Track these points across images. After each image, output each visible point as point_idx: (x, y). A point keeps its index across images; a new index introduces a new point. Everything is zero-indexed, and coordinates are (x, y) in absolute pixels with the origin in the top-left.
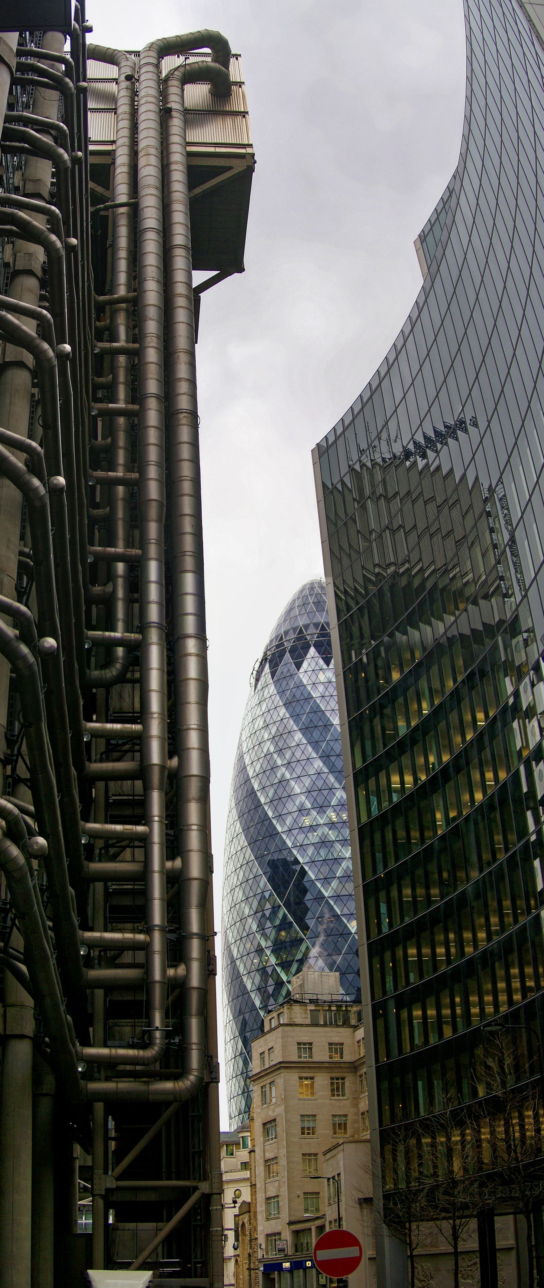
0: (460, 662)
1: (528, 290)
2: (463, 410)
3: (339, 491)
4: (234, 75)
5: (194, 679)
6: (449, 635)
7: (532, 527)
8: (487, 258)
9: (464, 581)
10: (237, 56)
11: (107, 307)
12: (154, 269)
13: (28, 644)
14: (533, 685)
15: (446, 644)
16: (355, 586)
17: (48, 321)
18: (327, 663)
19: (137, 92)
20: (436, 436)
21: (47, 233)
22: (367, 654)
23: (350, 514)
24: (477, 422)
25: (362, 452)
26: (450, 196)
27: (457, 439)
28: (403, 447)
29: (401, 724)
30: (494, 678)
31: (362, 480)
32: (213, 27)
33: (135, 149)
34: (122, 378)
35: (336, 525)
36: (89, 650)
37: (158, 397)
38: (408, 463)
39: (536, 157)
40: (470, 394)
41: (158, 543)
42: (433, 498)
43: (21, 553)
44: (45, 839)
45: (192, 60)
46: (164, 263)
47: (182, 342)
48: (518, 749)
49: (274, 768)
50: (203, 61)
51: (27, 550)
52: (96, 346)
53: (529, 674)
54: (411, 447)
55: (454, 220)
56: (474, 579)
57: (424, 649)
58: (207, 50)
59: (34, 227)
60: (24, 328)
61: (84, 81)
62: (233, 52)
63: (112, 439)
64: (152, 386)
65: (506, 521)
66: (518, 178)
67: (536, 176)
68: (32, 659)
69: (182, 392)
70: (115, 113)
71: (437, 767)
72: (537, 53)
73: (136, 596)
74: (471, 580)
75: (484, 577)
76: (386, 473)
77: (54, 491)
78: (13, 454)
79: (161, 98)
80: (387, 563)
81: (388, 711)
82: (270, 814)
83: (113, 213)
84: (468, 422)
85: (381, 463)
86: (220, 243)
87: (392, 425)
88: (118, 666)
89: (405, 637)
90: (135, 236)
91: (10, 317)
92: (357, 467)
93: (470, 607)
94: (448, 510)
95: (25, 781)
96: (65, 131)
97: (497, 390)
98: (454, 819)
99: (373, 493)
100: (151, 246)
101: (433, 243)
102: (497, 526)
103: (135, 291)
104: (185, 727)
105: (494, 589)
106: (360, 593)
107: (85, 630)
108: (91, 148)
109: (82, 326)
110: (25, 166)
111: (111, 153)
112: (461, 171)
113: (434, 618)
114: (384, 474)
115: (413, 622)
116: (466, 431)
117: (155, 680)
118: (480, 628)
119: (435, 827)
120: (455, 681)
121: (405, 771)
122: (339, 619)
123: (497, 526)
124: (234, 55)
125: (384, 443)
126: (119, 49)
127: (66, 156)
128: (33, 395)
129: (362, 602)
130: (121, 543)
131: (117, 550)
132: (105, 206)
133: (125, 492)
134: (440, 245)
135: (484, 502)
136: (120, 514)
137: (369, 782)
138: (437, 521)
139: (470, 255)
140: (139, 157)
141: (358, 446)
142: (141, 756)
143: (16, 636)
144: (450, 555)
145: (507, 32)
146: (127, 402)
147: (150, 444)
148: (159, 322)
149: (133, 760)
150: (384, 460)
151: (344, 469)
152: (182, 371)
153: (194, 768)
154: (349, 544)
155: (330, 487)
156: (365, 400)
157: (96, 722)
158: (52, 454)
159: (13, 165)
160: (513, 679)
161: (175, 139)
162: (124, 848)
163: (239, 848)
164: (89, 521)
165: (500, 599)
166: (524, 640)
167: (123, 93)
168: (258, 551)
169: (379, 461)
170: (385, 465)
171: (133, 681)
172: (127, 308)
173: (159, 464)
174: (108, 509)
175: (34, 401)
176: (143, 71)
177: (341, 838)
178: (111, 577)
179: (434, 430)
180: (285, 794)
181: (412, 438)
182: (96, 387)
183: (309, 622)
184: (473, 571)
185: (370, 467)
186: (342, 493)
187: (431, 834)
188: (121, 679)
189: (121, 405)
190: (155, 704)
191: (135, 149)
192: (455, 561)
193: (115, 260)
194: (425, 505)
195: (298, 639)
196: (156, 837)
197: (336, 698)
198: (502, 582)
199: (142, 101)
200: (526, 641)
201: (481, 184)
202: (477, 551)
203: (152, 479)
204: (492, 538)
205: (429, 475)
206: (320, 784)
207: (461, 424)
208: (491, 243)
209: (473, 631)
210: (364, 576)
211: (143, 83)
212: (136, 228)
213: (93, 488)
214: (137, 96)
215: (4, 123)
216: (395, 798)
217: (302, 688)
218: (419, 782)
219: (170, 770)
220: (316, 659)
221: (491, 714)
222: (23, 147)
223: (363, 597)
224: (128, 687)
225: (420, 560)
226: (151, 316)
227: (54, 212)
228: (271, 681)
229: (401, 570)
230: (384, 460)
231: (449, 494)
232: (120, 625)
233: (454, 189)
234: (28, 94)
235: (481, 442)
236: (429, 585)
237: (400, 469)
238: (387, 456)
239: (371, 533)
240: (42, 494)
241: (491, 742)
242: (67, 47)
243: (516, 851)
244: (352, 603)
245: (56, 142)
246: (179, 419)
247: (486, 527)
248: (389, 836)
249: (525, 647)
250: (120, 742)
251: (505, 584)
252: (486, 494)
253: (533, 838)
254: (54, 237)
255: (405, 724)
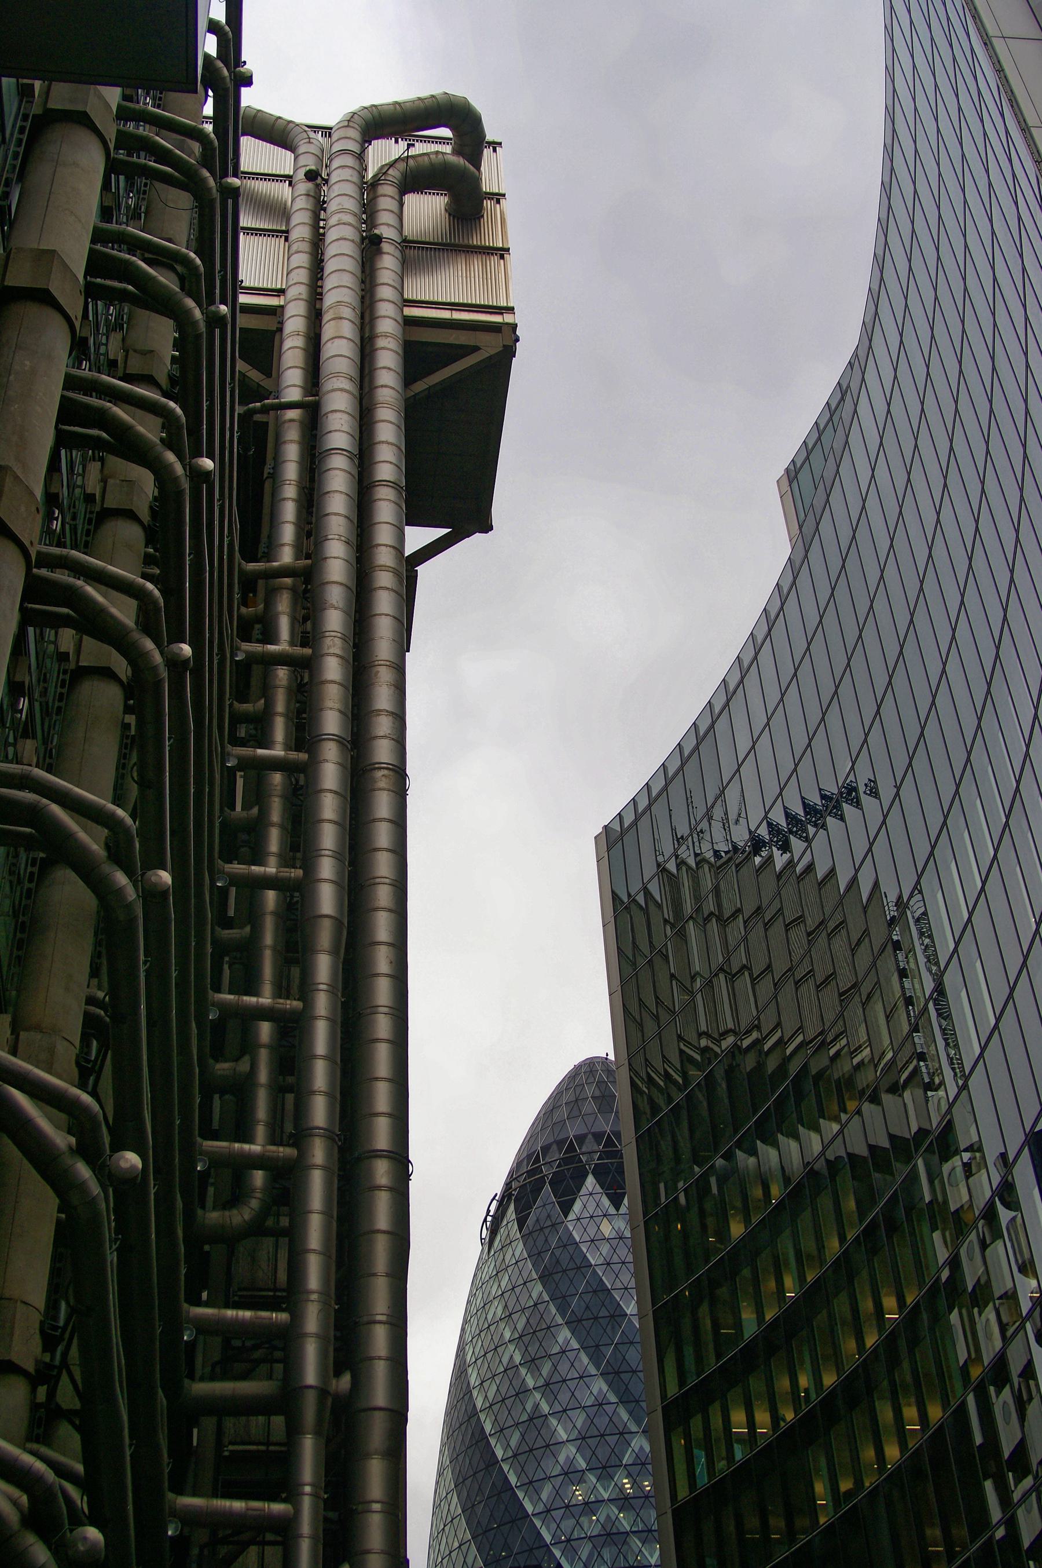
0: (850, 1204)
1: (970, 559)
2: (852, 768)
3: (641, 907)
4: (489, 183)
5: (384, 1232)
6: (830, 1155)
7: (975, 966)
8: (901, 507)
9: (855, 1061)
10: (495, 145)
11: (261, 583)
12: (341, 521)
13: (91, 1163)
14: (984, 1246)
15: (825, 1172)
16: (665, 1070)
17: (155, 602)
18: (617, 1203)
19: (324, 202)
20: (806, 813)
21: (160, 448)
22: (686, 1190)
23: (658, 946)
24: (877, 789)
25: (680, 840)
26: (842, 399)
27: (842, 818)
28: (750, 832)
29: (748, 1316)
30: (913, 1234)
31: (679, 889)
32: (458, 89)
33: (318, 306)
34: (280, 707)
35: (634, 964)
36: (204, 1175)
37: (340, 741)
38: (758, 860)
39: (995, 325)
40: (865, 741)
41: (332, 990)
42: (800, 919)
43: (91, 1001)
44: (101, 1531)
45: (420, 148)
46: (359, 511)
47: (383, 648)
48: (961, 1363)
49: (523, 1392)
50: (437, 153)
51: (100, 995)
52: (238, 649)
53: (977, 1227)
54: (763, 832)
55: (847, 442)
56: (873, 1058)
57: (787, 1180)
58: (445, 132)
59: (139, 436)
60: (114, 611)
61: (235, 175)
62: (489, 138)
63: (260, 810)
64: (332, 722)
65: (928, 957)
66: (960, 363)
67: (993, 359)
68: (95, 1189)
69: (382, 734)
70: (286, 239)
71: (813, 1396)
72: (1007, 132)
73: (290, 1079)
74: (866, 1061)
75: (889, 1055)
76: (720, 876)
77: (153, 896)
78: (85, 829)
79: (364, 216)
80: (722, 1029)
81: (723, 1292)
82: (513, 1479)
83: (277, 418)
84: (862, 788)
85: (712, 859)
86: (453, 479)
87: (732, 795)
88: (254, 1204)
89: (752, 1160)
90: (313, 462)
91: (89, 589)
92: (672, 866)
93: (867, 1107)
94: (826, 940)
95: (68, 1415)
96: (197, 268)
97: (913, 732)
98: (849, 1494)
99: (698, 910)
100: (338, 479)
101: (809, 484)
102: (912, 965)
103: (308, 556)
104: (365, 1319)
105: (909, 1075)
106: (675, 1083)
107: (199, 1139)
108: (243, 299)
109: (216, 614)
110: (128, 323)
111: (276, 313)
112: (862, 354)
113: (803, 1126)
114: (716, 878)
115: (766, 1132)
116: (858, 804)
117: (315, 1232)
118: (885, 1143)
119: (813, 1511)
120: (842, 1239)
121: (756, 1404)
122: (637, 1127)
123: (912, 965)
124: (490, 143)
125: (717, 826)
126: (297, 121)
127: (198, 314)
128: (126, 727)
129: (679, 1097)
130: (267, 988)
131: (261, 1000)
132: (263, 406)
133: (277, 902)
134: (821, 487)
135: (889, 925)
136: (269, 939)
137: (692, 1422)
138: (807, 959)
139: (872, 503)
140: (324, 322)
141: (673, 830)
142: (285, 1371)
143: (70, 1148)
144: (829, 1016)
145: (957, 96)
146: (287, 747)
147: (323, 821)
148: (346, 613)
149: (270, 1377)
150: (716, 853)
151: (650, 870)
152: (382, 698)
153: (380, 1396)
154: (657, 998)
155: (626, 900)
156: (686, 753)
157: (207, 1304)
158: (152, 834)
159: (107, 319)
160: (947, 1234)
161: (385, 292)
162: (244, 1546)
163: (456, 1544)
164: (214, 949)
165: (919, 1092)
166: (964, 1165)
167: (301, 203)
168: (502, 1008)
169: (709, 855)
170: (719, 863)
171: (278, 1233)
172: (294, 585)
173: (338, 856)
174: (248, 929)
175: (127, 737)
176: (335, 164)
177: (641, 1527)
178: (248, 1046)
179: (804, 803)
180: (540, 1443)
181: (766, 817)
182: (237, 719)
183: (585, 1131)
184: (870, 1045)
185: (694, 865)
186: (646, 911)
187: (807, 1522)
188: (257, 1229)
189: (278, 752)
190: (314, 1275)
191: (318, 306)
192: (839, 1027)
193: (276, 501)
194: (787, 931)
195: (565, 1161)
196: (306, 1527)
197: (631, 1267)
198: (922, 1064)
199: (333, 221)
200: (967, 1167)
201: (896, 377)
202: (878, 1010)
203: (326, 880)
204: (903, 988)
205: (793, 880)
206: (602, 1422)
207: (850, 793)
208: (909, 480)
209: (872, 1148)
210: (681, 1052)
211: (336, 187)
212: (314, 447)
213: (224, 892)
214: (325, 210)
215: (93, 241)
216: (739, 1454)
217: (571, 1249)
218: (782, 1424)
219: (337, 1397)
220: (597, 1197)
221: (909, 1299)
222: (125, 290)
223: (680, 1089)
224: (268, 1242)
225: (779, 1025)
226: (334, 602)
227: (172, 412)
228: (518, 1235)
229: (746, 1043)
230: (716, 853)
231: (828, 910)
232: (261, 1131)
233: (848, 386)
234: (138, 192)
235: (884, 822)
236: (794, 1068)
237: (744, 870)
238: (723, 847)
239: (693, 978)
240: (130, 899)
241: (911, 1352)
242: (208, 110)
243: (969, 1558)
244: (661, 1101)
245: (182, 289)
246: (375, 780)
247: (893, 967)
248: (730, 1527)
249: (967, 1178)
250: (248, 1343)
251: (927, 1066)
252: (892, 911)
253: (1000, 1533)
254: (171, 457)
255: (754, 1316)
